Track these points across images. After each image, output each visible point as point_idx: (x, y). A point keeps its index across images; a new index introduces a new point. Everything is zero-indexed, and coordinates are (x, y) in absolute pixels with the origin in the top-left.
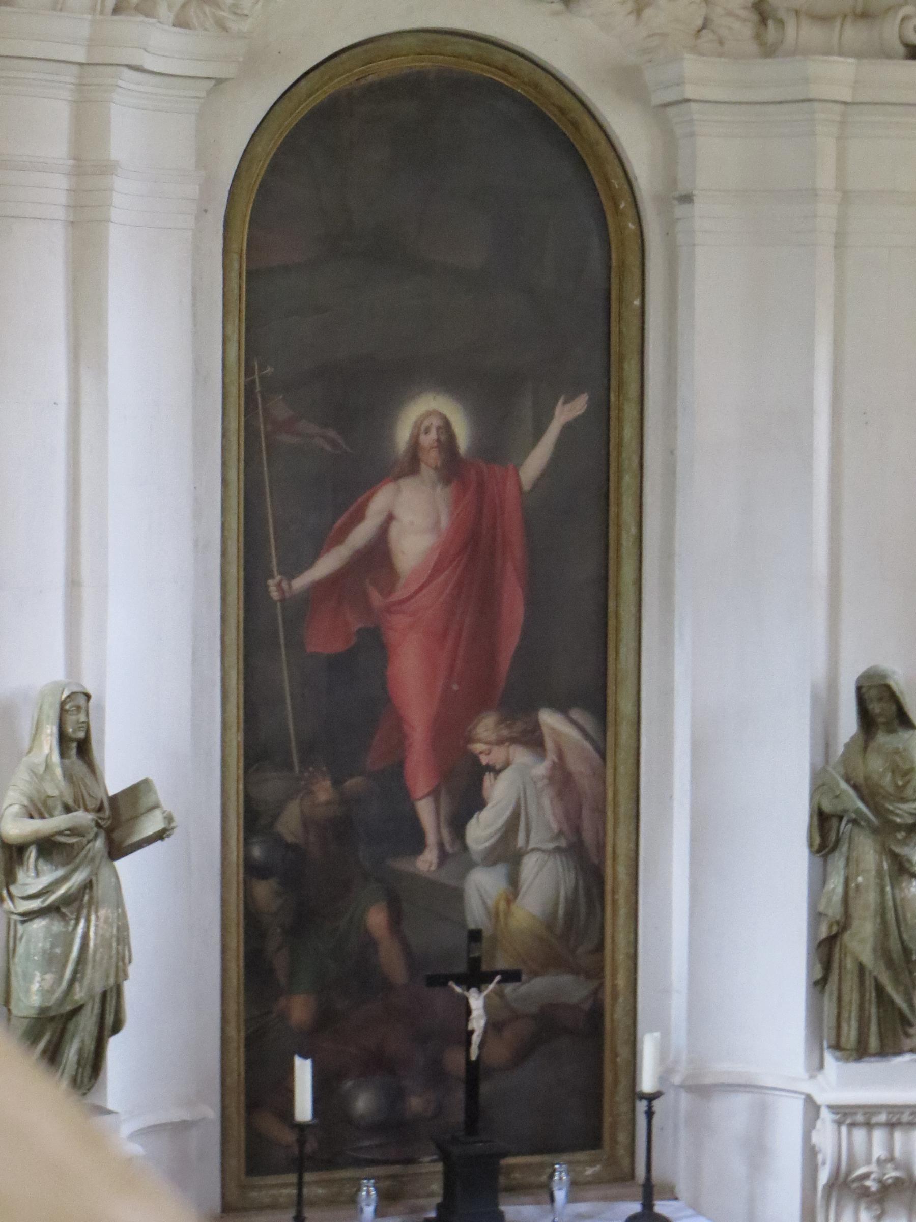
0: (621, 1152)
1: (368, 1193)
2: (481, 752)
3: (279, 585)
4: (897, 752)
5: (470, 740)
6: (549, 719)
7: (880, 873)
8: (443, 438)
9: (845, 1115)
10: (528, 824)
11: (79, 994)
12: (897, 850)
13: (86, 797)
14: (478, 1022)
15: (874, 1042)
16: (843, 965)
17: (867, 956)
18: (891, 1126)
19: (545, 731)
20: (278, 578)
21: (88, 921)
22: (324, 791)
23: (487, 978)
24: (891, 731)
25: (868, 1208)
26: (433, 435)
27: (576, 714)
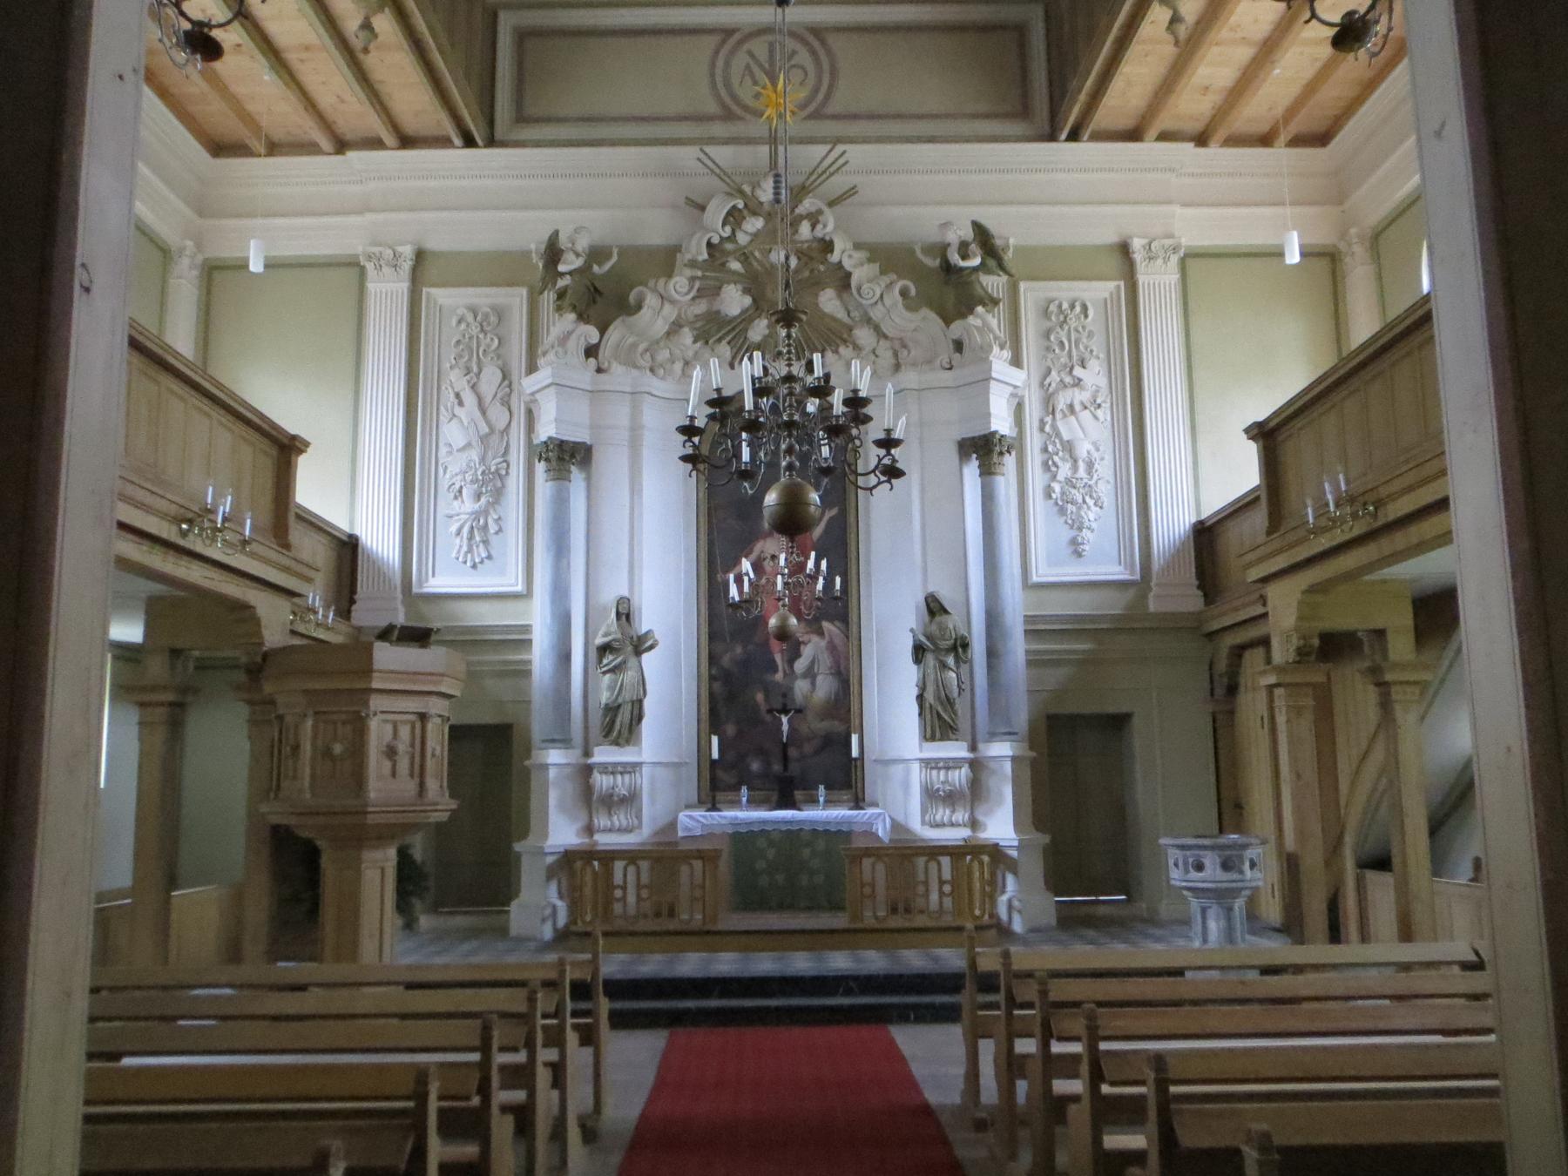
0: (859, 790)
6: (826, 625)
7: (935, 667)
9: (928, 764)
11: (620, 700)
12: (942, 658)
14: (785, 727)
15: (938, 735)
18: (947, 768)
24: (941, 615)
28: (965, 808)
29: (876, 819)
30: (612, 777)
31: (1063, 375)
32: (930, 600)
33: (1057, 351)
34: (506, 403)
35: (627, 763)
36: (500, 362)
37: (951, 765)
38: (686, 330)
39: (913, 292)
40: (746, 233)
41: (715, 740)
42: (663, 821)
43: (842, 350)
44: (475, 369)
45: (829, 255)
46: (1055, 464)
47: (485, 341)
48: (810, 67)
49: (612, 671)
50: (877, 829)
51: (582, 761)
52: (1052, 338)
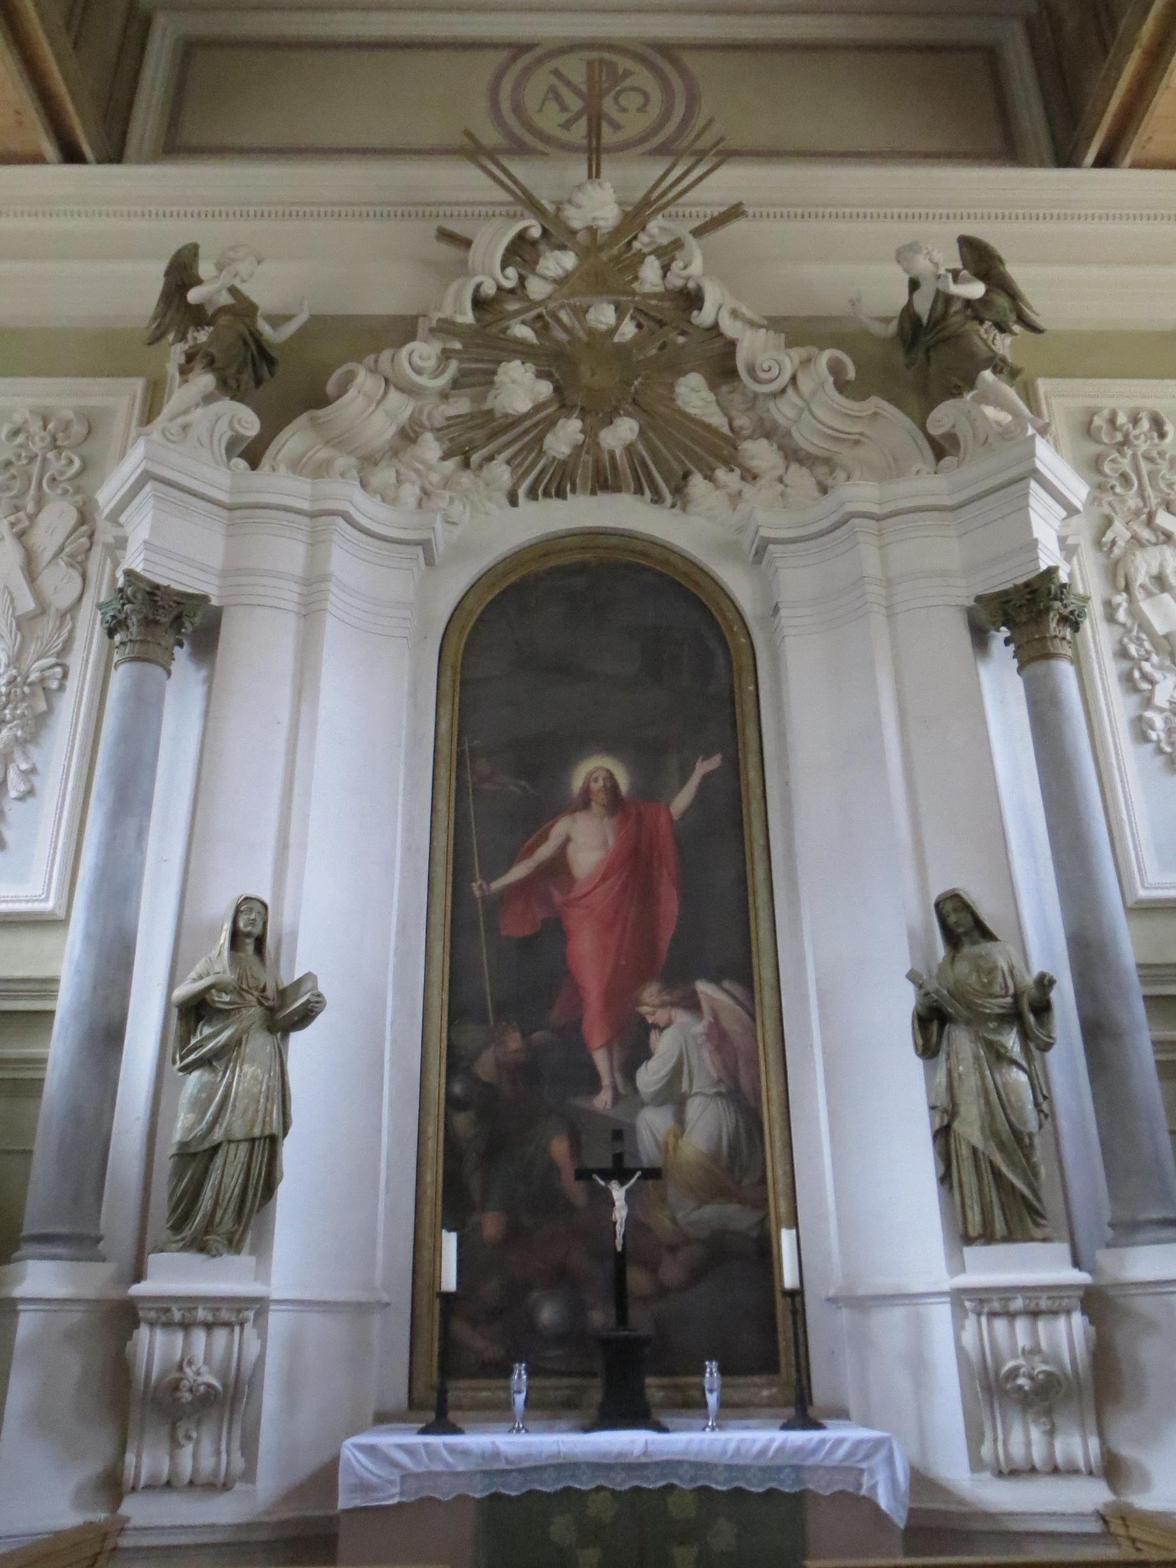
1: (520, 1376)
2: (647, 1013)
3: (480, 886)
4: (980, 956)
5: (638, 1003)
6: (704, 988)
7: (977, 1058)
8: (609, 785)
9: (981, 1301)
10: (690, 1073)
12: (991, 1037)
13: (249, 976)
14: (620, 1213)
15: (999, 1226)
16: (959, 1154)
17: (977, 1139)
19: (702, 997)
20: (479, 882)
21: (233, 1072)
22: (514, 1042)
23: (629, 1174)
25: (1035, 1422)
26: (601, 783)
27: (727, 984)
28: (1082, 1426)
29: (867, 1457)
30: (179, 1338)
31: (1135, 526)
32: (948, 906)
33: (1118, 490)
34: (79, 563)
35: (223, 1299)
36: (78, 498)
37: (1044, 1304)
38: (429, 437)
39: (851, 374)
40: (544, 278)
41: (450, 1242)
42: (308, 1464)
43: (721, 474)
44: (30, 507)
45: (695, 313)
46: (1145, 677)
47: (54, 467)
48: (656, 96)
49: (205, 1062)
50: (874, 1487)
51: (114, 1294)
52: (1107, 468)
